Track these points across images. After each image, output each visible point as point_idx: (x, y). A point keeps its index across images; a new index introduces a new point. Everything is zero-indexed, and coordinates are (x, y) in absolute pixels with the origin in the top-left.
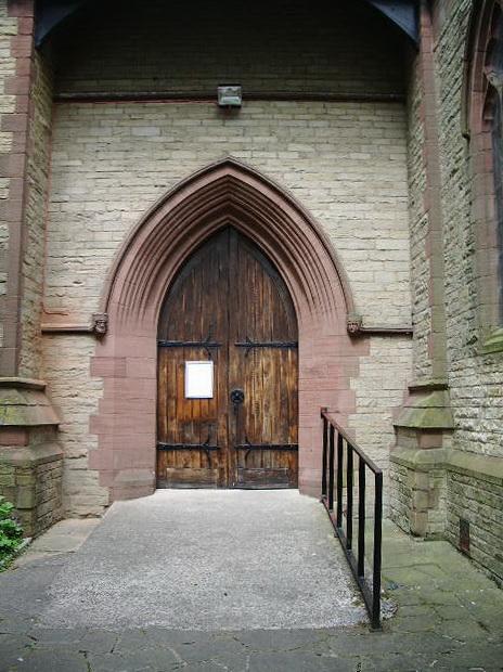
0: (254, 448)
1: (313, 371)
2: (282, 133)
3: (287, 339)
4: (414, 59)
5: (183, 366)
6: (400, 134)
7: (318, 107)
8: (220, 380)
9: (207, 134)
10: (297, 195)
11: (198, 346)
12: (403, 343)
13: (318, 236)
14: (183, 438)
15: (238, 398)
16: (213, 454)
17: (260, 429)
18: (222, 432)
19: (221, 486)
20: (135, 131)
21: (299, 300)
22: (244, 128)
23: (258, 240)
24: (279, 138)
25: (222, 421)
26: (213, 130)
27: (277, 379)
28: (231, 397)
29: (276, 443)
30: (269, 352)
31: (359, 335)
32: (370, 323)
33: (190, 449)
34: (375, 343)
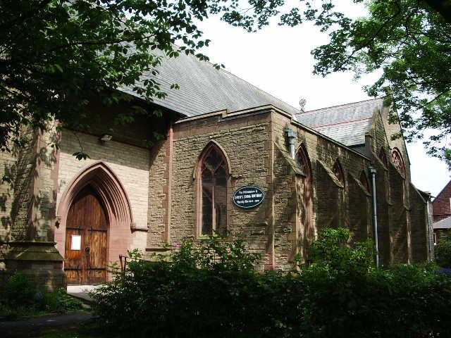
0: (92, 269)
1: (117, 242)
2: (117, 154)
3: (104, 227)
4: (138, 152)
5: (71, 237)
6: (148, 161)
7: (127, 147)
8: (83, 243)
9: (95, 150)
10: (119, 177)
11: (76, 229)
12: (145, 233)
13: (125, 194)
14: (70, 266)
15: (88, 250)
16: (79, 272)
17: (94, 262)
18: (83, 263)
19: (82, 284)
20: (73, 143)
21: (111, 215)
22: (106, 150)
23: (107, 188)
24: (116, 156)
25: (82, 259)
26: (97, 149)
27: (100, 244)
28: (86, 249)
29: (99, 267)
30: (98, 233)
31: (133, 230)
32: (138, 226)
33: (72, 270)
34: (137, 232)
